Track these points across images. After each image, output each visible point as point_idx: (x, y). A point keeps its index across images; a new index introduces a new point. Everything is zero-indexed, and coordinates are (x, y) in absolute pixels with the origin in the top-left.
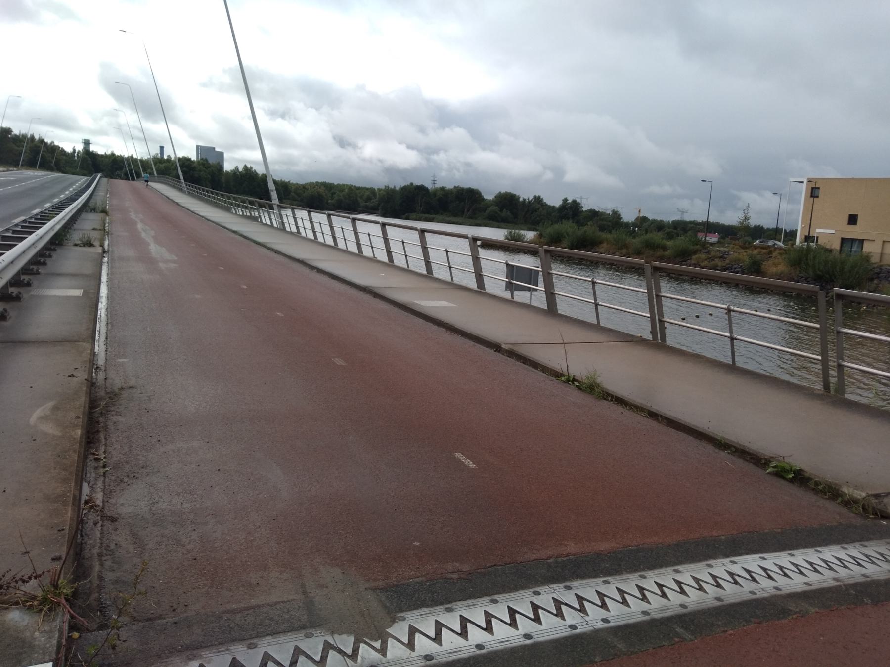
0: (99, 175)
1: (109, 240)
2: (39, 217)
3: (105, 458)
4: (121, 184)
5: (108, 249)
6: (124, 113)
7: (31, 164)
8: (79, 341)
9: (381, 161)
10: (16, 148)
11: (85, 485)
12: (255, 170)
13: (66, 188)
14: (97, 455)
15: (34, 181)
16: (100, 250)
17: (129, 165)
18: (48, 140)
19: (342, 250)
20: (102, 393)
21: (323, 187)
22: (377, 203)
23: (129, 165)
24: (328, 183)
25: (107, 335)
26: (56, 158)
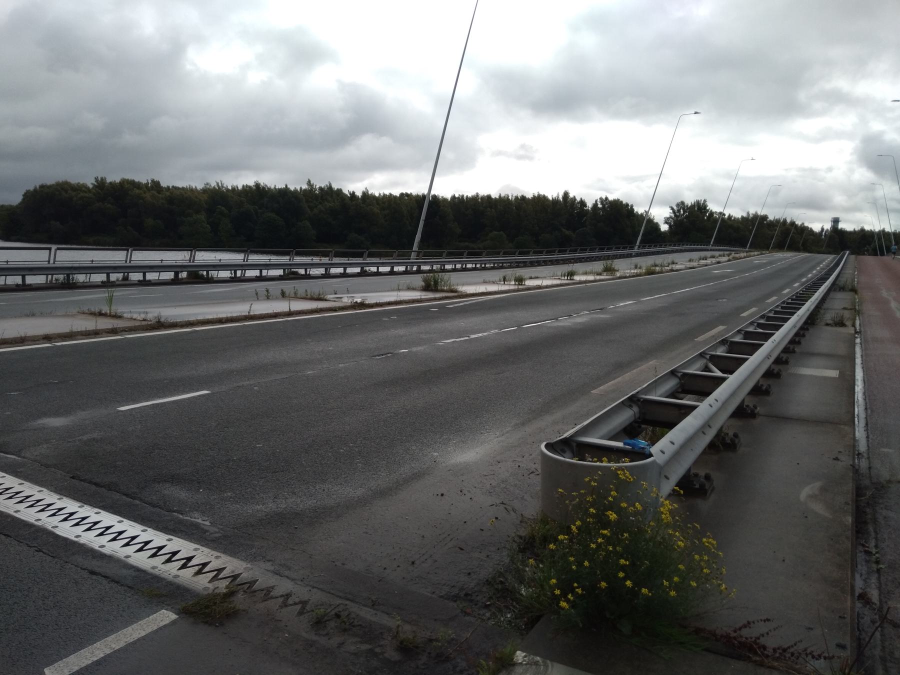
0: (848, 252)
1: (860, 319)
2: (794, 297)
3: (877, 553)
4: (869, 260)
5: (860, 329)
6: (883, 186)
7: (780, 246)
8: (840, 424)
10: (770, 232)
11: (857, 576)
13: (814, 268)
14: (868, 547)
15: (783, 262)
16: (852, 331)
17: (880, 239)
18: (799, 223)
20: (867, 482)
23: (880, 239)
25: (867, 420)
26: (804, 238)
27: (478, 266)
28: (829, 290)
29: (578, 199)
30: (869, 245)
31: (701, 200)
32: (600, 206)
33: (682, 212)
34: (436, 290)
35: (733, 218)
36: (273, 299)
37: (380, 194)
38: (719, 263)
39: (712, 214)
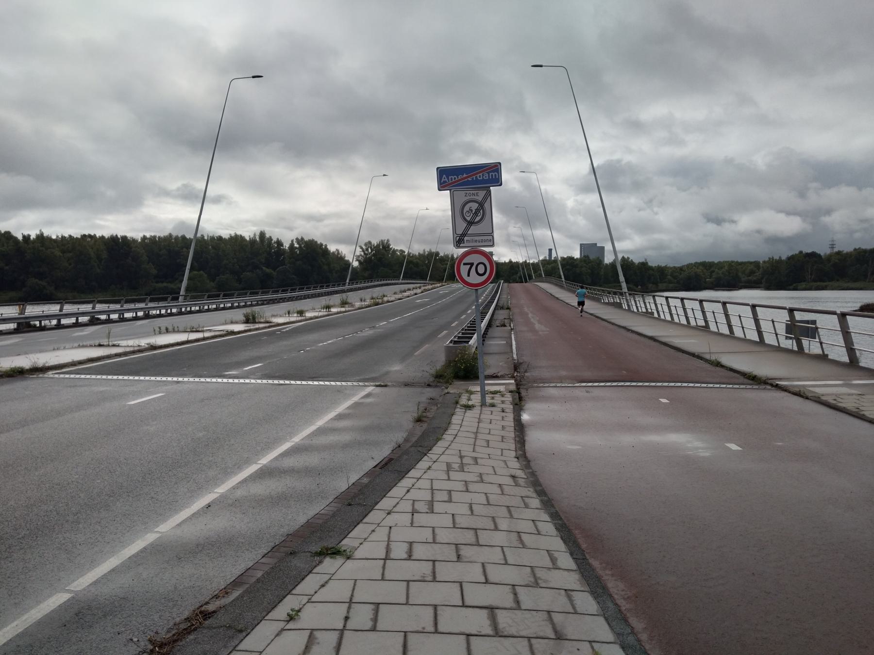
0: (502, 281)
9: (759, 232)
10: (442, 266)
12: (632, 260)
17: (523, 269)
19: (663, 320)
21: (701, 267)
22: (761, 276)
23: (523, 269)
24: (708, 262)
27: (163, 312)
28: (495, 309)
29: (275, 239)
30: (517, 274)
31: (385, 240)
32: (296, 245)
33: (370, 251)
34: (254, 322)
35: (411, 255)
36: (162, 333)
37: (57, 236)
38: (416, 294)
39: (395, 251)
